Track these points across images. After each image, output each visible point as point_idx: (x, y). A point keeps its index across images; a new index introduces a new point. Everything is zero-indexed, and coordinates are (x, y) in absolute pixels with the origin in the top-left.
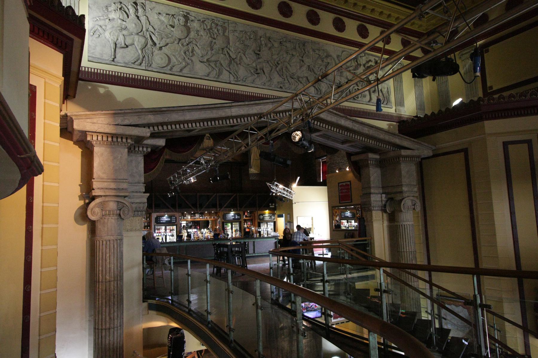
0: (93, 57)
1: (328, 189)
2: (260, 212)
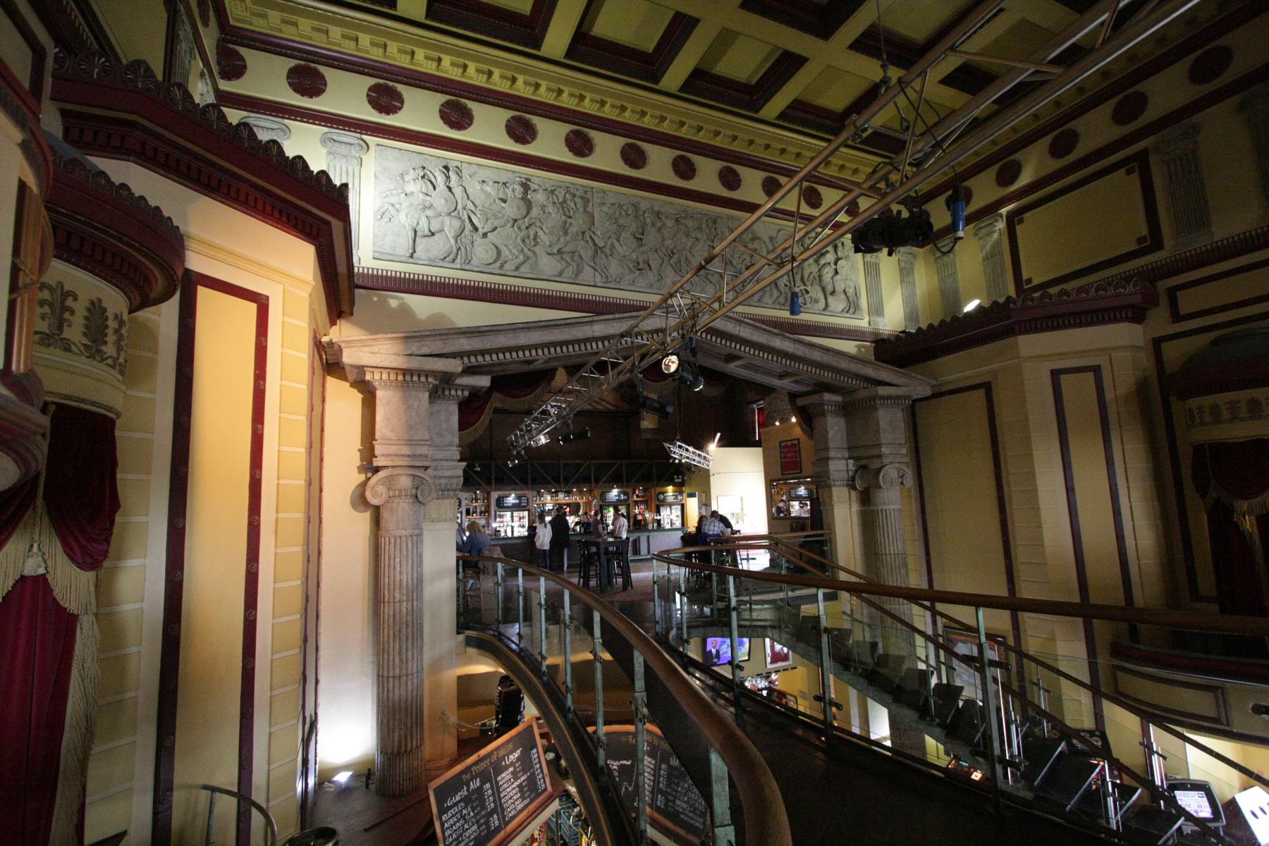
0: (381, 252)
1: (764, 451)
2: (659, 490)
